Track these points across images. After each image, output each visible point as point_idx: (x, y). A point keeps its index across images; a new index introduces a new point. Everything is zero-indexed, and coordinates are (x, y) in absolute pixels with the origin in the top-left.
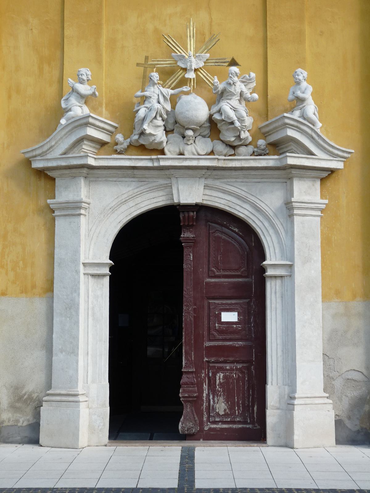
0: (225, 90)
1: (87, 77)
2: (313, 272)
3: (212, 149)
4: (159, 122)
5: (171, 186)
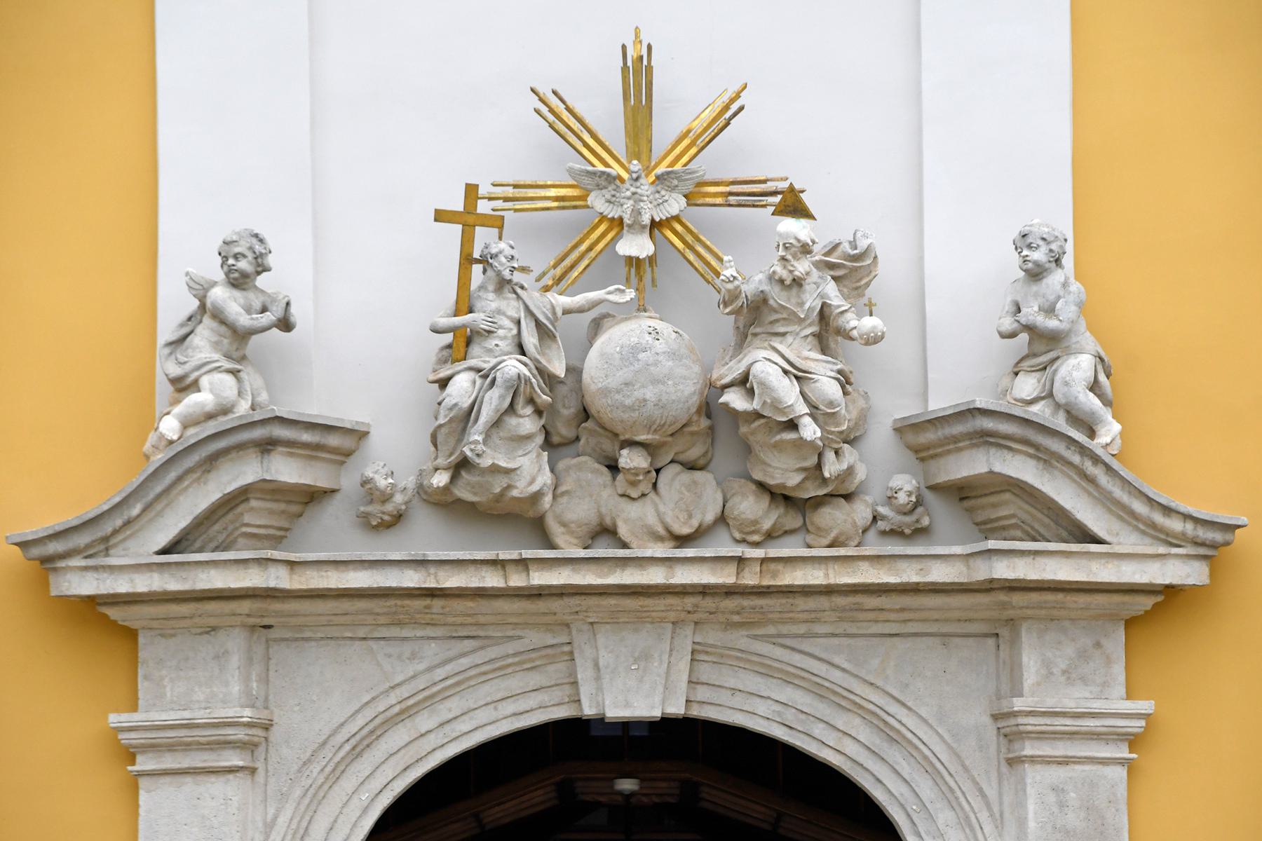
0: (765, 301)
1: (257, 262)
3: (718, 509)
4: (527, 423)
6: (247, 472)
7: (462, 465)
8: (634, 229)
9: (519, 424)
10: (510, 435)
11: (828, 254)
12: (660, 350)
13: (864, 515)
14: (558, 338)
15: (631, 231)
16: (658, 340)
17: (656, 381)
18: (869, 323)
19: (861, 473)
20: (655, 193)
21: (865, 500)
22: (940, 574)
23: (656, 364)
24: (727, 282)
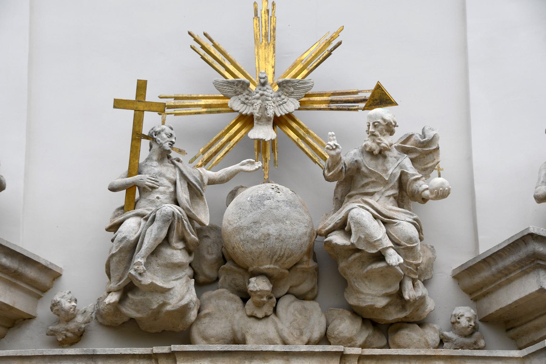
0: (358, 170)
3: (323, 330)
8: (262, 122)
9: (173, 254)
10: (165, 263)
11: (405, 142)
12: (281, 199)
13: (433, 338)
14: (204, 197)
15: (260, 123)
16: (279, 192)
17: (277, 220)
19: (430, 304)
20: (277, 97)
21: (434, 327)
23: (277, 208)
24: (331, 150)
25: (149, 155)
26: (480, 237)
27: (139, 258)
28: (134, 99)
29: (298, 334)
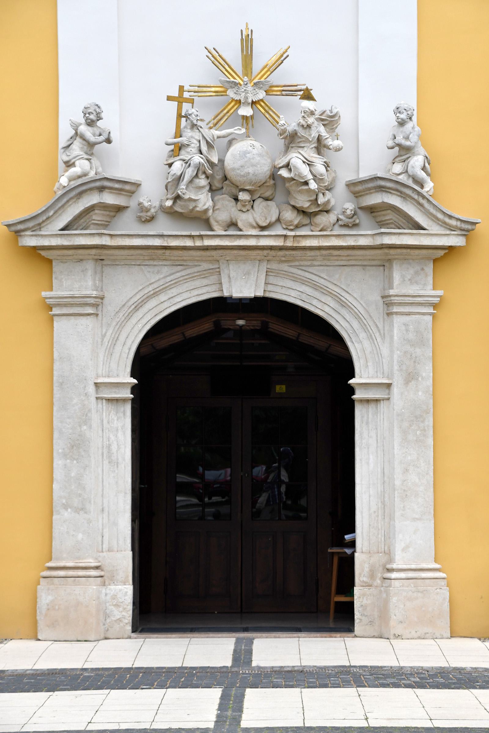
0: (296, 134)
2: (420, 393)
4: (202, 181)
5: (219, 272)
6: (93, 199)
7: (177, 198)
11: (321, 115)
14: (215, 148)
17: (253, 165)
18: (336, 143)
19: (333, 202)
22: (362, 242)
23: (253, 159)
25: (186, 125)
26: (360, 164)
27: (183, 186)
28: (178, 96)
29: (264, 219)
